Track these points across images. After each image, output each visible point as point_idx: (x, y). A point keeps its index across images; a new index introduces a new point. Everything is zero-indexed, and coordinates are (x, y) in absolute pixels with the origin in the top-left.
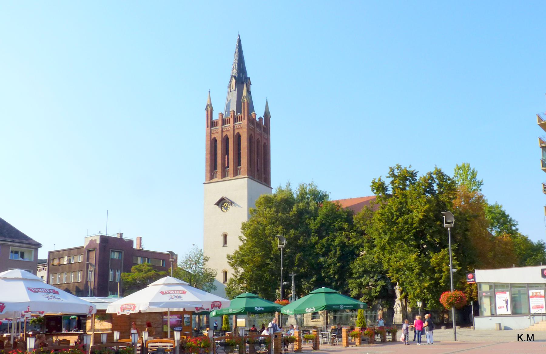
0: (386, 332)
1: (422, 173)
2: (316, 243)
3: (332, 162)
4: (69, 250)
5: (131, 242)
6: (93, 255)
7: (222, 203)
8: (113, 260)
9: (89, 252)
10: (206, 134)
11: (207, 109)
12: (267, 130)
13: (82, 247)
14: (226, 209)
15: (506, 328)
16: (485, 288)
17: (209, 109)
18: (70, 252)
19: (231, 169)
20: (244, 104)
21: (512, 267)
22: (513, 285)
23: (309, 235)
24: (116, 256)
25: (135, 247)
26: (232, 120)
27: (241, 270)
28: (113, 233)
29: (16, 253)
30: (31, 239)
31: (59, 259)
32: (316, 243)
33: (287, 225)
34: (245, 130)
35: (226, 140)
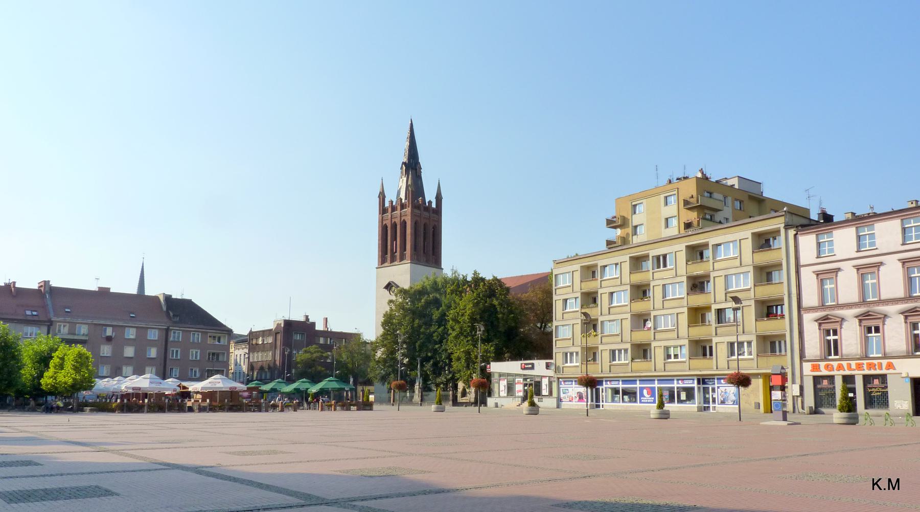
1: (489, 277)
2: (434, 332)
3: (468, 253)
4: (263, 331)
5: (313, 324)
6: (279, 337)
8: (296, 341)
9: (276, 334)
10: (140, 389)
12: (438, 211)
16: (496, 376)
17: (382, 196)
18: (264, 333)
19: (398, 254)
20: (416, 188)
22: (509, 375)
26: (399, 208)
27: (496, 342)
28: (298, 317)
29: (214, 337)
32: (434, 332)
35: (394, 226)
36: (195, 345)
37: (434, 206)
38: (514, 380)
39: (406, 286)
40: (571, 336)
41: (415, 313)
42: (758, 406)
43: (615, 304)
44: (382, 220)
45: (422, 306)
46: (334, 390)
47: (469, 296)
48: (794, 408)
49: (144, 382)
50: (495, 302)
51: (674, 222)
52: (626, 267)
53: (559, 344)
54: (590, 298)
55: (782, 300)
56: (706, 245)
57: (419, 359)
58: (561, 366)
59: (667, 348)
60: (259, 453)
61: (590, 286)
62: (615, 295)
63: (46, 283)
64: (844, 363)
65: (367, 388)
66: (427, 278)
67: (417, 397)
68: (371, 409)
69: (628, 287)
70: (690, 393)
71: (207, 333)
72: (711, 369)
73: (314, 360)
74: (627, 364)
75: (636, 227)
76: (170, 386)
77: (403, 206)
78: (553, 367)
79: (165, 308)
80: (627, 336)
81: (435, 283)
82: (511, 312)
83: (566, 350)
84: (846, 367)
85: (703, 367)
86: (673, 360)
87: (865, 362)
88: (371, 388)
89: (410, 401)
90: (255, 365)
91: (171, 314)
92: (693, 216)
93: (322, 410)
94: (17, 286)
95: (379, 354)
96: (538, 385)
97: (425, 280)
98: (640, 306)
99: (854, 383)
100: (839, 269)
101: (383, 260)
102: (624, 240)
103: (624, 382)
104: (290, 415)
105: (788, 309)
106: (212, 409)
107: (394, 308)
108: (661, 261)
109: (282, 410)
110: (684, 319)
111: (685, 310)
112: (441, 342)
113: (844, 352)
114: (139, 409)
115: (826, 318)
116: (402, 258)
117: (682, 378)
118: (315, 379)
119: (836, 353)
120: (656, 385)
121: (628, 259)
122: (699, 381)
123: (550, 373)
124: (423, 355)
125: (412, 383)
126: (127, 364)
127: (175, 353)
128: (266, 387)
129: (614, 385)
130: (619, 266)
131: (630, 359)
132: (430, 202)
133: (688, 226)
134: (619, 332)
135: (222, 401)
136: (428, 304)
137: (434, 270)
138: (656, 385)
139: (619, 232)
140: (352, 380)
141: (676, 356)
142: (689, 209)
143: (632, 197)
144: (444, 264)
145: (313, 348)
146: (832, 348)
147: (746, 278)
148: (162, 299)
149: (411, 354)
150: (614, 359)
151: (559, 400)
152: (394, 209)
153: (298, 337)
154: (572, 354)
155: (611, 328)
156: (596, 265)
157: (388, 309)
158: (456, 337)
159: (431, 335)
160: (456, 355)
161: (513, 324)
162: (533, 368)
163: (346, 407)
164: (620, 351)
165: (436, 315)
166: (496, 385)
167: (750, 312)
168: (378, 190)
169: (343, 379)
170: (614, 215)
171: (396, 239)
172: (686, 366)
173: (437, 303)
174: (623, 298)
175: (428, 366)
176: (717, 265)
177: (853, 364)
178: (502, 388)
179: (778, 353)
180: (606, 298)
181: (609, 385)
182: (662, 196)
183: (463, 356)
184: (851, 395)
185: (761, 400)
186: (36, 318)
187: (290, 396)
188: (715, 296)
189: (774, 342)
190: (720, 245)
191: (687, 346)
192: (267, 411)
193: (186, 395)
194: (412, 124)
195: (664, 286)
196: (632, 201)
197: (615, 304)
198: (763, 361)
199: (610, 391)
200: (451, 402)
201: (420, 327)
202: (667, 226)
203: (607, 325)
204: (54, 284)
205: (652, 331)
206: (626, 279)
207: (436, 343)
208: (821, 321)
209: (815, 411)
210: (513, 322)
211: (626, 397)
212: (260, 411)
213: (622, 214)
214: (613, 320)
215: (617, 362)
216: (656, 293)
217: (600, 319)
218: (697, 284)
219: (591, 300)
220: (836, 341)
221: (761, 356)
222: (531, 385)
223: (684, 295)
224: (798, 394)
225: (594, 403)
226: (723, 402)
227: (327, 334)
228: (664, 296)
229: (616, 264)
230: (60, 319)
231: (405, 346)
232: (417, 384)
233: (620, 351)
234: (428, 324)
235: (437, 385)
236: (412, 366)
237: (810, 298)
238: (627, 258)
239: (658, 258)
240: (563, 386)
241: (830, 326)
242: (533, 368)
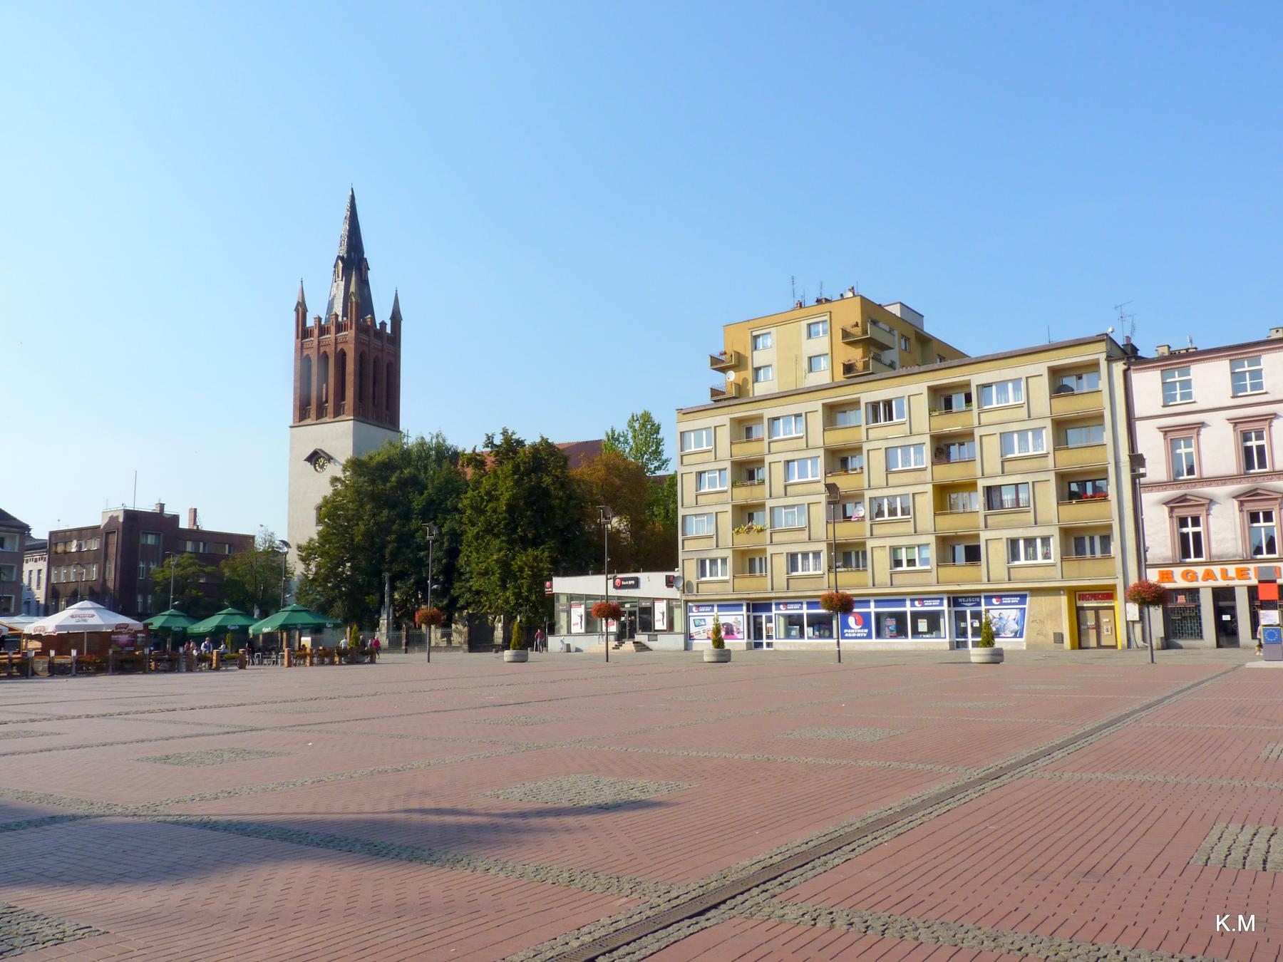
0: (361, 654)
3: (446, 408)
4: (80, 530)
5: (175, 518)
6: (114, 539)
7: (315, 458)
8: (146, 546)
9: (108, 534)
11: (297, 310)
12: (395, 339)
13: (98, 527)
14: (322, 467)
15: (578, 650)
16: (563, 600)
17: (301, 310)
18: (81, 534)
20: (360, 301)
21: (587, 574)
23: (409, 520)
24: (151, 540)
25: (184, 524)
26: (333, 329)
28: (146, 505)
30: (15, 519)
31: (65, 543)
33: (380, 500)
34: (352, 346)
37: (388, 330)
40: (712, 532)
42: (1059, 638)
43: (705, 489)
45: (391, 488)
48: (1129, 639)
50: (547, 480)
51: (824, 363)
52: (817, 420)
53: (689, 545)
54: (746, 471)
55: (1106, 471)
56: (759, 418)
57: (387, 575)
58: (694, 582)
59: (894, 550)
64: (1217, 569)
69: (821, 453)
70: (934, 620)
72: (979, 582)
74: (821, 577)
75: (757, 370)
77: (340, 328)
82: (570, 498)
83: (703, 556)
84: (1218, 575)
85: (962, 577)
86: (905, 567)
87: (1252, 566)
90: (61, 589)
92: (856, 355)
96: (648, 611)
97: (387, 446)
99: (1234, 599)
100: (1202, 424)
102: (741, 391)
103: (811, 605)
105: (1118, 485)
110: (727, 520)
111: (729, 508)
113: (1214, 551)
115: (1183, 499)
116: (338, 412)
119: (1198, 553)
121: (925, 392)
122: (748, 605)
123: (674, 593)
124: (396, 567)
129: (793, 610)
132: (383, 324)
134: (804, 524)
136: (403, 484)
137: (390, 434)
139: (732, 376)
141: (911, 562)
142: (849, 343)
144: (404, 424)
146: (1189, 546)
147: (814, 465)
150: (703, 574)
151: (689, 637)
152: (323, 330)
154: (714, 561)
158: (477, 537)
164: (805, 555)
165: (418, 502)
166: (563, 616)
167: (1049, 493)
168: (295, 299)
172: (932, 577)
176: (985, 418)
177: (1232, 570)
179: (1088, 555)
180: (778, 470)
181: (783, 610)
182: (804, 324)
184: (1226, 618)
185: (1065, 628)
188: (985, 461)
189: (1083, 538)
190: (777, 419)
192: (189, 670)
194: (353, 197)
196: (752, 329)
197: (705, 489)
198: (1073, 567)
205: (868, 522)
208: (1172, 504)
209: (1167, 644)
219: (745, 475)
220: (1197, 536)
221: (1068, 560)
224: (1137, 618)
227: (197, 535)
229: (798, 416)
233: (805, 555)
237: (1156, 469)
240: (694, 614)
241: (1187, 513)
242: (636, 584)
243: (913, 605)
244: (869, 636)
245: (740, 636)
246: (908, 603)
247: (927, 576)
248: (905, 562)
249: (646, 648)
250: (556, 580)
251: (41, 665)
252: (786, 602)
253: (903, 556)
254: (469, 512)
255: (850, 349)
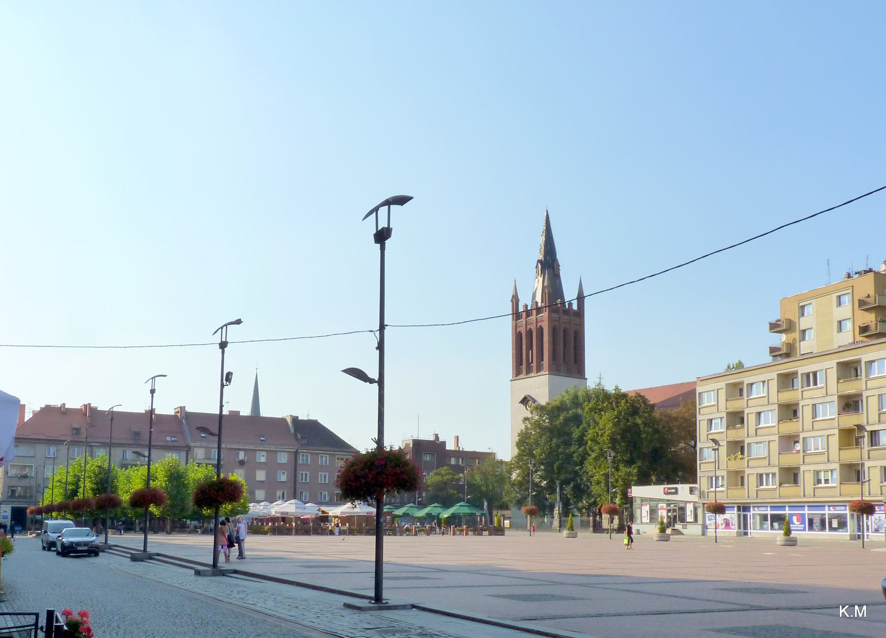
2: (574, 453)
3: (619, 362)
5: (444, 443)
10: (287, 513)
11: (512, 301)
12: (580, 314)
16: (638, 501)
17: (515, 300)
19: (534, 365)
20: (554, 289)
22: (651, 500)
34: (546, 323)
36: (322, 468)
37: (575, 307)
38: (657, 506)
39: (543, 400)
40: (766, 455)
41: (553, 432)
44: (516, 327)
46: (465, 515)
47: (607, 416)
49: (288, 507)
50: (639, 421)
51: (848, 325)
52: (774, 385)
54: (736, 418)
57: (558, 482)
60: (396, 578)
61: (736, 405)
62: (762, 414)
63: (182, 409)
65: (500, 513)
66: (567, 392)
67: (556, 523)
68: (503, 535)
69: (776, 407)
71: (334, 455)
73: (446, 483)
74: (775, 490)
75: (804, 331)
76: (311, 510)
77: (539, 310)
78: (697, 493)
79: (292, 431)
80: (775, 459)
81: (576, 397)
82: (656, 431)
86: (823, 485)
88: (507, 513)
89: (549, 528)
91: (299, 436)
92: (870, 318)
93: (454, 534)
94: (156, 412)
95: (514, 476)
96: (683, 509)
97: (565, 394)
98: (789, 427)
101: (518, 372)
103: (772, 508)
104: (422, 538)
106: (351, 532)
107: (529, 426)
108: (811, 378)
109: (416, 535)
110: (835, 441)
111: (836, 431)
112: (581, 463)
114: (287, 532)
116: (539, 369)
117: (833, 504)
118: (447, 505)
120: (806, 511)
121: (775, 377)
123: (695, 498)
124: (562, 477)
125: (552, 508)
126: (259, 488)
127: (304, 476)
128: (399, 512)
130: (766, 384)
131: (778, 484)
132: (570, 304)
133: (864, 329)
135: (360, 525)
136: (567, 421)
138: (806, 511)
139: (784, 337)
140: (486, 504)
141: (827, 481)
143: (799, 298)
145: (444, 470)
148: (289, 421)
149: (549, 474)
150: (761, 484)
151: (705, 527)
152: (528, 313)
153: (427, 458)
155: (758, 451)
156: (742, 383)
157: (523, 427)
158: (596, 459)
159: (570, 456)
160: (595, 478)
161: (658, 445)
162: (676, 493)
163: (478, 532)
164: (767, 475)
165: (576, 434)
166: (638, 511)
169: (475, 503)
170: (779, 318)
171: (531, 348)
173: (577, 420)
174: (770, 419)
175: (568, 490)
176: (870, 384)
178: (644, 514)
182: (834, 296)
183: (602, 479)
186: (175, 444)
187: (421, 520)
190: (874, 361)
191: (838, 470)
192: (401, 535)
193: (325, 519)
195: (814, 406)
199: (758, 518)
200: (591, 529)
201: (558, 446)
202: (840, 330)
203: (754, 447)
204: (189, 409)
205: (801, 454)
206: (774, 398)
207: (577, 465)
210: (658, 440)
211: (776, 525)
212: (395, 535)
213: (787, 317)
214: (761, 443)
215: (764, 487)
216: (805, 413)
217: (747, 441)
218: (850, 404)
222: (674, 511)
223: (835, 416)
225: (742, 530)
226: (877, 531)
228: (814, 415)
229: (764, 382)
230: (198, 444)
231: (542, 467)
232: (557, 508)
233: (767, 475)
234: (568, 444)
235: (580, 510)
236: (551, 489)
238: (774, 375)
239: (808, 375)
242: (676, 493)
243: (829, 510)
244: (804, 530)
245: (733, 527)
246: (827, 508)
247: (837, 491)
248: (823, 481)
249: (680, 533)
250: (633, 488)
251: (336, 530)
252: (758, 505)
253: (822, 477)
254: (590, 442)
255: (865, 313)
